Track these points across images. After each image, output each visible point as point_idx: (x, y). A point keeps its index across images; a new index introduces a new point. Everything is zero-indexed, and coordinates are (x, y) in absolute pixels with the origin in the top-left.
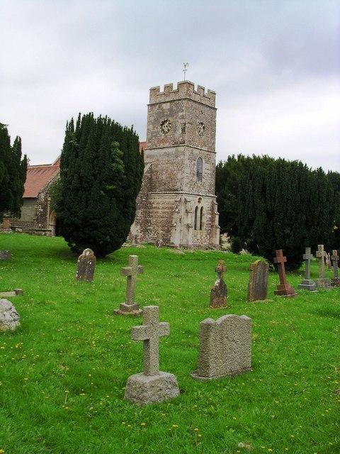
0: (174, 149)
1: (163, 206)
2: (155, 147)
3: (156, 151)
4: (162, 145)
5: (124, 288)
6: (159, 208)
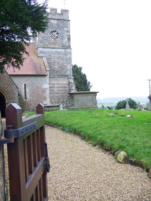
0: (63, 50)
1: (58, 86)
2: (46, 47)
3: (48, 50)
4: (52, 46)
5: (64, 74)
6: (54, 87)
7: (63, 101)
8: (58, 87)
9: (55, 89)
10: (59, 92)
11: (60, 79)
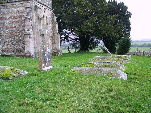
1: (10, 15)
7: (19, 38)
8: (10, 18)
9: (7, 21)
10: (13, 24)
11: (12, 4)
